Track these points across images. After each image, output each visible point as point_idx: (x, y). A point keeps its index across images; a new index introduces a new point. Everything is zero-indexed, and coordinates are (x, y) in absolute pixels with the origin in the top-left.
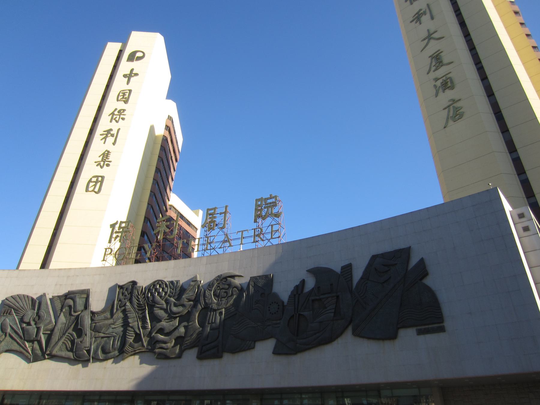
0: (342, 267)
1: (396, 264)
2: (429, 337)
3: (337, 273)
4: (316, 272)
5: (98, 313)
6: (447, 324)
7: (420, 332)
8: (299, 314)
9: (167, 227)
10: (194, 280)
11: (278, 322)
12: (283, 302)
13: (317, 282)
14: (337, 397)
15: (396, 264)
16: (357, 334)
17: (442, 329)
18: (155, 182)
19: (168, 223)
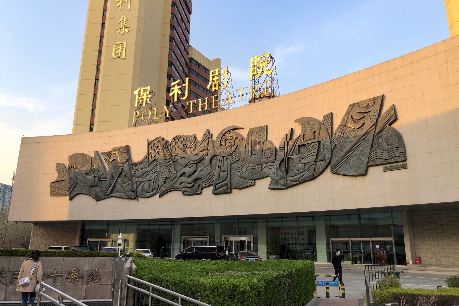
0: (324, 116)
1: (370, 112)
2: (393, 173)
3: (319, 122)
4: (305, 122)
5: (135, 164)
6: (409, 162)
7: (386, 170)
8: (289, 158)
9: (180, 89)
10: (30, 147)
11: (272, 164)
12: (276, 148)
13: (303, 130)
14: (325, 220)
15: (370, 112)
16: (335, 172)
17: (405, 167)
18: (171, 51)
19: (180, 87)
